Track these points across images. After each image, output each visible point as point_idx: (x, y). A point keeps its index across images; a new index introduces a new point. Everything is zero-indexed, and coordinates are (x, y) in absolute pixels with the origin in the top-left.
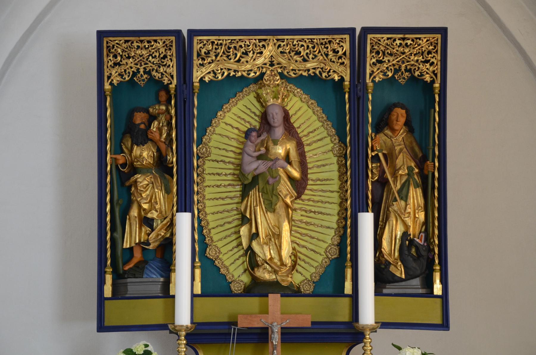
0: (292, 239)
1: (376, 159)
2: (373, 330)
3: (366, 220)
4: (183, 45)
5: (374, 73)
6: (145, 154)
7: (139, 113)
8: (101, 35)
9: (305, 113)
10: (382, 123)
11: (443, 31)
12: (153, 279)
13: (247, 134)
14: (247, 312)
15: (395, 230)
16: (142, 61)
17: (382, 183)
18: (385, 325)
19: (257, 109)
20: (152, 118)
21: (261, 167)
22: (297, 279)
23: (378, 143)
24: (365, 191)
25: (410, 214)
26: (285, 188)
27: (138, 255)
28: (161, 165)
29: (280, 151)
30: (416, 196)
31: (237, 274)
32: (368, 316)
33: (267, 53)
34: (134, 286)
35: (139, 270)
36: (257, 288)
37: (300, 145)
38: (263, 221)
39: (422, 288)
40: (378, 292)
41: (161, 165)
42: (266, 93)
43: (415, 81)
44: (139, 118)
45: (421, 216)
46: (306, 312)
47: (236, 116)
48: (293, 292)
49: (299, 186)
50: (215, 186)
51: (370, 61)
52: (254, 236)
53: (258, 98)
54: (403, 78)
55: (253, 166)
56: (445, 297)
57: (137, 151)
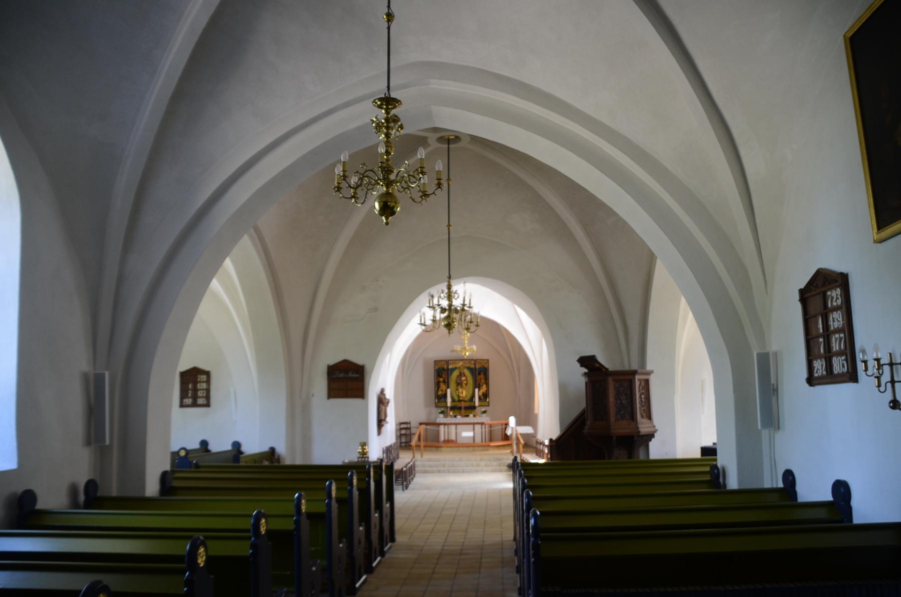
0: (464, 393)
3: (477, 390)
4: (447, 362)
6: (441, 379)
7: (252, 446)
9: (467, 372)
10: (479, 374)
15: (481, 391)
23: (478, 378)
24: (477, 385)
25: (484, 388)
31: (456, 399)
32: (477, 404)
36: (460, 401)
39: (267, 531)
46: (467, 404)
47: (456, 373)
50: (453, 384)
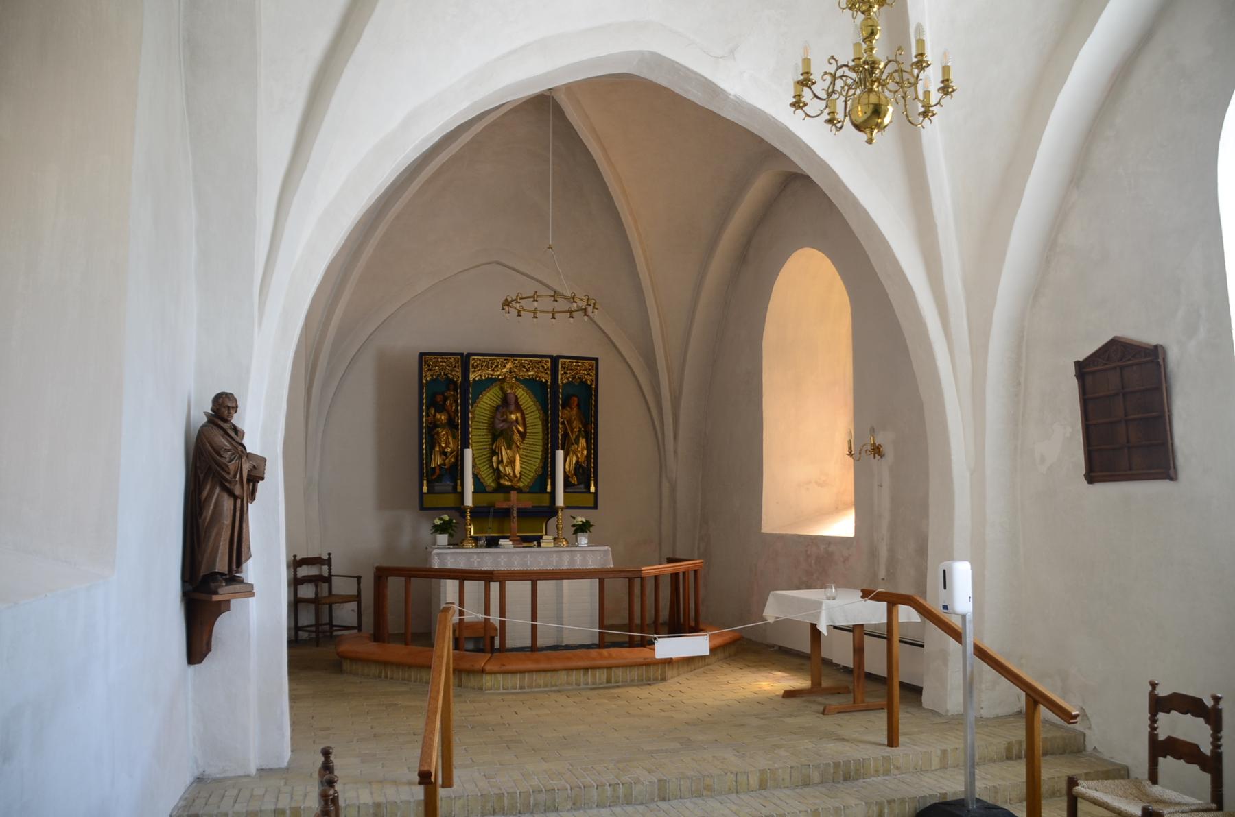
1: (563, 423)
2: (562, 508)
3: (560, 454)
4: (465, 360)
5: (562, 379)
8: (422, 355)
9: (525, 397)
11: (596, 360)
12: (447, 484)
13: (497, 408)
14: (499, 501)
16: (443, 368)
17: (566, 435)
18: (568, 507)
19: (500, 394)
20: (446, 399)
21: (505, 425)
22: (521, 484)
23: (564, 414)
24: (554, 440)
26: (517, 437)
27: (438, 471)
28: (451, 424)
29: (513, 417)
30: (582, 442)
31: (489, 482)
32: (560, 501)
33: (508, 366)
34: (438, 487)
35: (440, 479)
37: (523, 415)
38: (505, 454)
40: (565, 492)
41: (451, 424)
42: (506, 386)
43: (583, 384)
44: (439, 398)
45: (585, 452)
47: (489, 399)
48: (520, 491)
49: (523, 435)
50: (478, 433)
51: (560, 373)
52: (500, 462)
53: (502, 389)
54: (577, 382)
55: (500, 425)
56: (596, 494)
57: (438, 416)
